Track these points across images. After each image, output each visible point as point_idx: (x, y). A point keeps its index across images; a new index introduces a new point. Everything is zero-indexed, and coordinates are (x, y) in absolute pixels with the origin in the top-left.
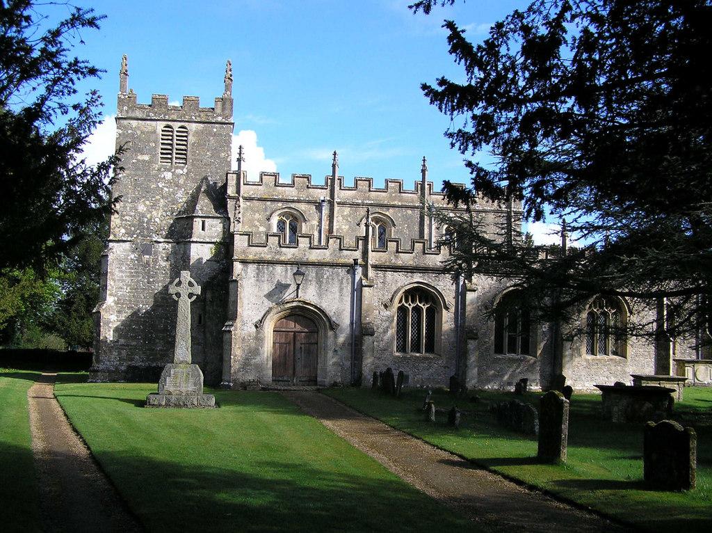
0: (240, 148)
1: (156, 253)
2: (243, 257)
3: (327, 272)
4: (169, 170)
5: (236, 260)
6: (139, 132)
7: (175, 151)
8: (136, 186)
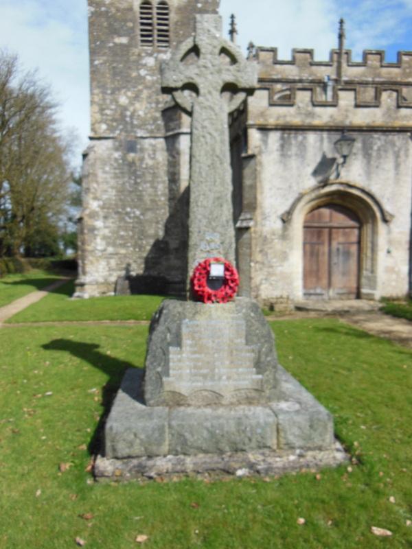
0: (232, 17)
1: (142, 150)
2: (261, 121)
3: (378, 140)
4: (150, 55)
5: (252, 126)
6: (113, 10)
7: (156, 33)
8: (115, 75)
